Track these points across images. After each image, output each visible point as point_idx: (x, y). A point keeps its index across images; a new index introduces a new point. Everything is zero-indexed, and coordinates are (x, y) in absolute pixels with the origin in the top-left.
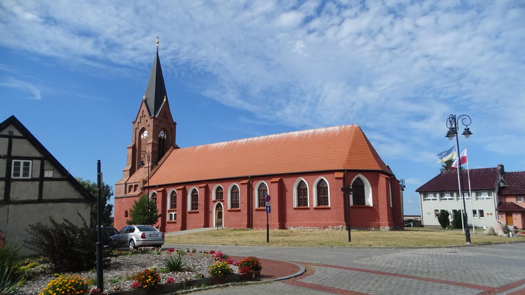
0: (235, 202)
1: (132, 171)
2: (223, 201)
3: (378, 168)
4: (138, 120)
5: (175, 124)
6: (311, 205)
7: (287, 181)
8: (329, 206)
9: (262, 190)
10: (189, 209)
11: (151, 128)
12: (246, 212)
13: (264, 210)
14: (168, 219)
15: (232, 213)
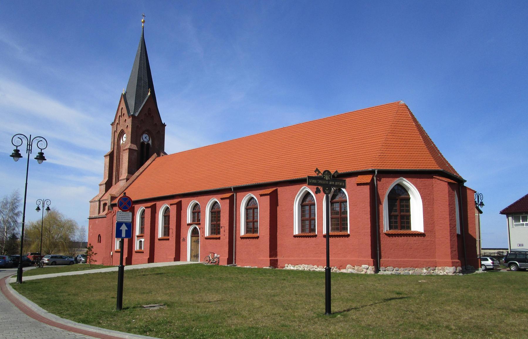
1: (108, 185)
2: (199, 224)
3: (435, 167)
4: (117, 122)
5: (164, 125)
6: (321, 231)
8: (349, 232)
10: (160, 234)
11: (130, 129)
14: (137, 247)
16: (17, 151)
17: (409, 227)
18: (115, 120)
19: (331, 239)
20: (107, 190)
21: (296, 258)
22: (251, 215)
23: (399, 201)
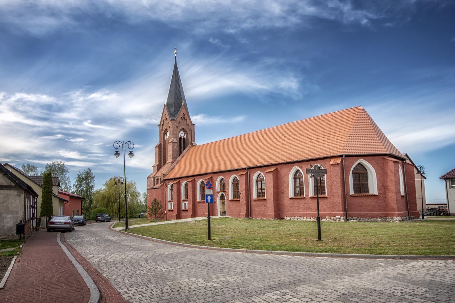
0: (260, 191)
4: (162, 123)
7: (282, 170)
9: (260, 181)
11: (171, 129)
12: (245, 202)
13: (171, 208)
14: (183, 208)
15: (234, 203)
16: (117, 152)
17: (368, 192)
18: (161, 123)
19: (316, 201)
20: (158, 171)
21: (292, 213)
22: (260, 185)
23: (361, 175)
